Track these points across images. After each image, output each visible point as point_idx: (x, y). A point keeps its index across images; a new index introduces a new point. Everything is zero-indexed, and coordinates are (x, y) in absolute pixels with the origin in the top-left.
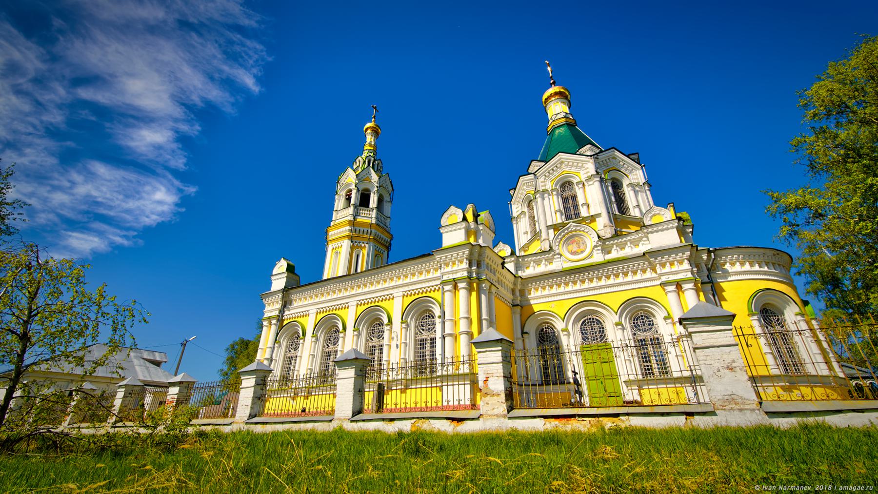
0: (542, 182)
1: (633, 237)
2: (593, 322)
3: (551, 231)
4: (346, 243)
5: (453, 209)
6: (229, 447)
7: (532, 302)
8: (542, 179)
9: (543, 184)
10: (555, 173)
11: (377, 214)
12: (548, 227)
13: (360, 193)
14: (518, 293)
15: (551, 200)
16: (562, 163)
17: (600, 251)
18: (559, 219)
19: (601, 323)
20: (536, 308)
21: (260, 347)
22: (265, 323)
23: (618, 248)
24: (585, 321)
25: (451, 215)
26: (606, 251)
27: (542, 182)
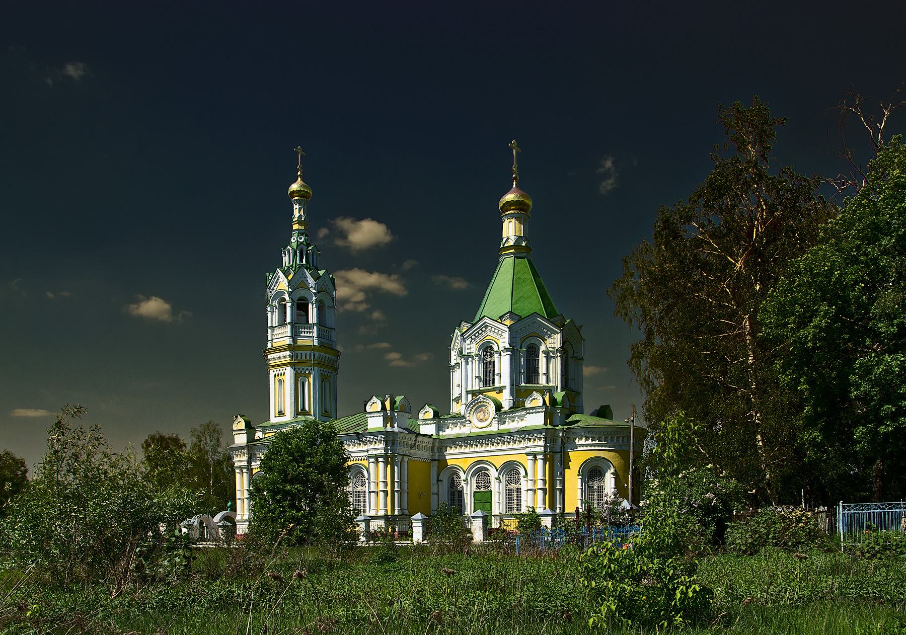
0: (468, 345)
1: (520, 413)
2: (485, 475)
3: (470, 396)
4: (289, 372)
5: (374, 399)
6: (554, 528)
7: (447, 457)
8: (468, 342)
9: (469, 347)
10: (480, 337)
11: (318, 330)
12: (468, 392)
13: (295, 304)
14: (436, 450)
15: (474, 364)
16: (486, 327)
17: (497, 422)
18: (476, 386)
19: (489, 476)
20: (450, 463)
21: (237, 489)
22: (237, 471)
23: (510, 421)
24: (479, 474)
25: (373, 403)
26: (502, 421)
27: (468, 345)
